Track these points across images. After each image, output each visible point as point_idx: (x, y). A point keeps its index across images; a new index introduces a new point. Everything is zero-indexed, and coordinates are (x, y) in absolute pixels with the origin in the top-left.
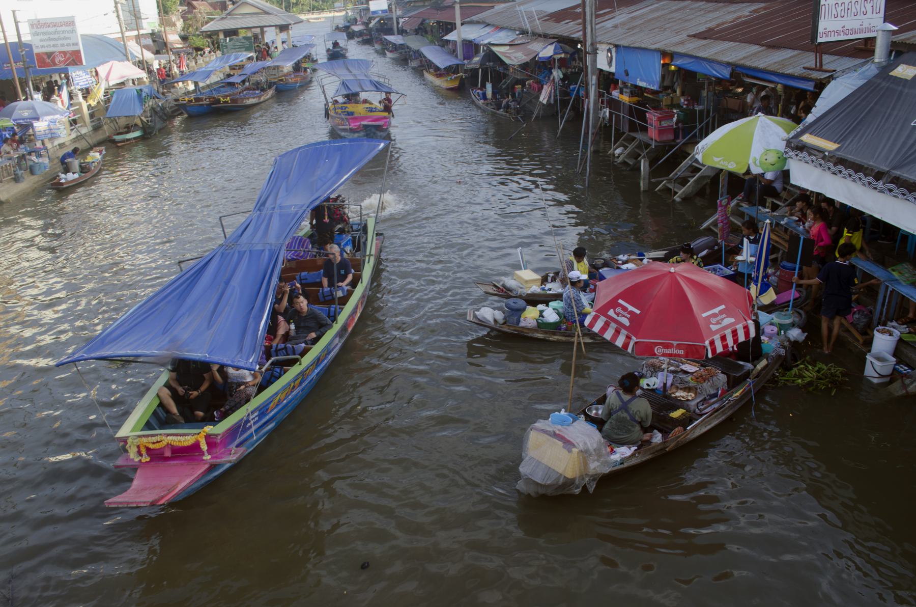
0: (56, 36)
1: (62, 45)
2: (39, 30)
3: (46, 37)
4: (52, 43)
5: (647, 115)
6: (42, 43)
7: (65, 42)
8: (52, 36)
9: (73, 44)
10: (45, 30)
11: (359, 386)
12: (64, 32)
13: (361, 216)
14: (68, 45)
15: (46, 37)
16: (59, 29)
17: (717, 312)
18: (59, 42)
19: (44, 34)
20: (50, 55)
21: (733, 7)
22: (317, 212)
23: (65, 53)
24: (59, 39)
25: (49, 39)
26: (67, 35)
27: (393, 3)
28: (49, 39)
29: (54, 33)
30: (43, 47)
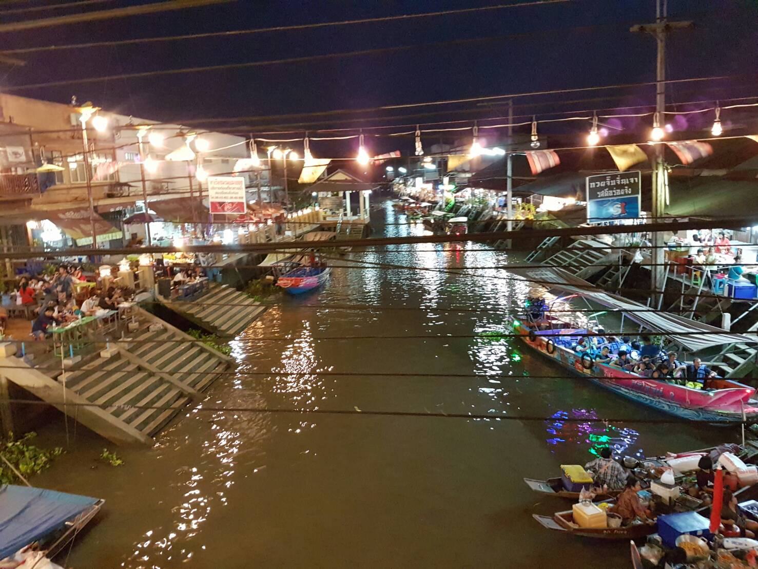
0: (228, 191)
1: (232, 198)
2: (215, 186)
3: (220, 191)
4: (224, 195)
5: (636, 262)
6: (217, 195)
7: (234, 196)
8: (225, 191)
9: (240, 198)
10: (220, 186)
11: (533, 149)
12: (234, 188)
13: (89, 152)
14: (236, 198)
15: (220, 191)
16: (231, 186)
17: (166, 338)
18: (229, 196)
19: (219, 188)
20: (221, 204)
21: (686, 462)
22: (132, 235)
23: (232, 203)
24: (229, 193)
25: (222, 193)
26: (236, 191)
27: (497, 258)
28: (222, 193)
29: (227, 188)
30: (217, 198)
